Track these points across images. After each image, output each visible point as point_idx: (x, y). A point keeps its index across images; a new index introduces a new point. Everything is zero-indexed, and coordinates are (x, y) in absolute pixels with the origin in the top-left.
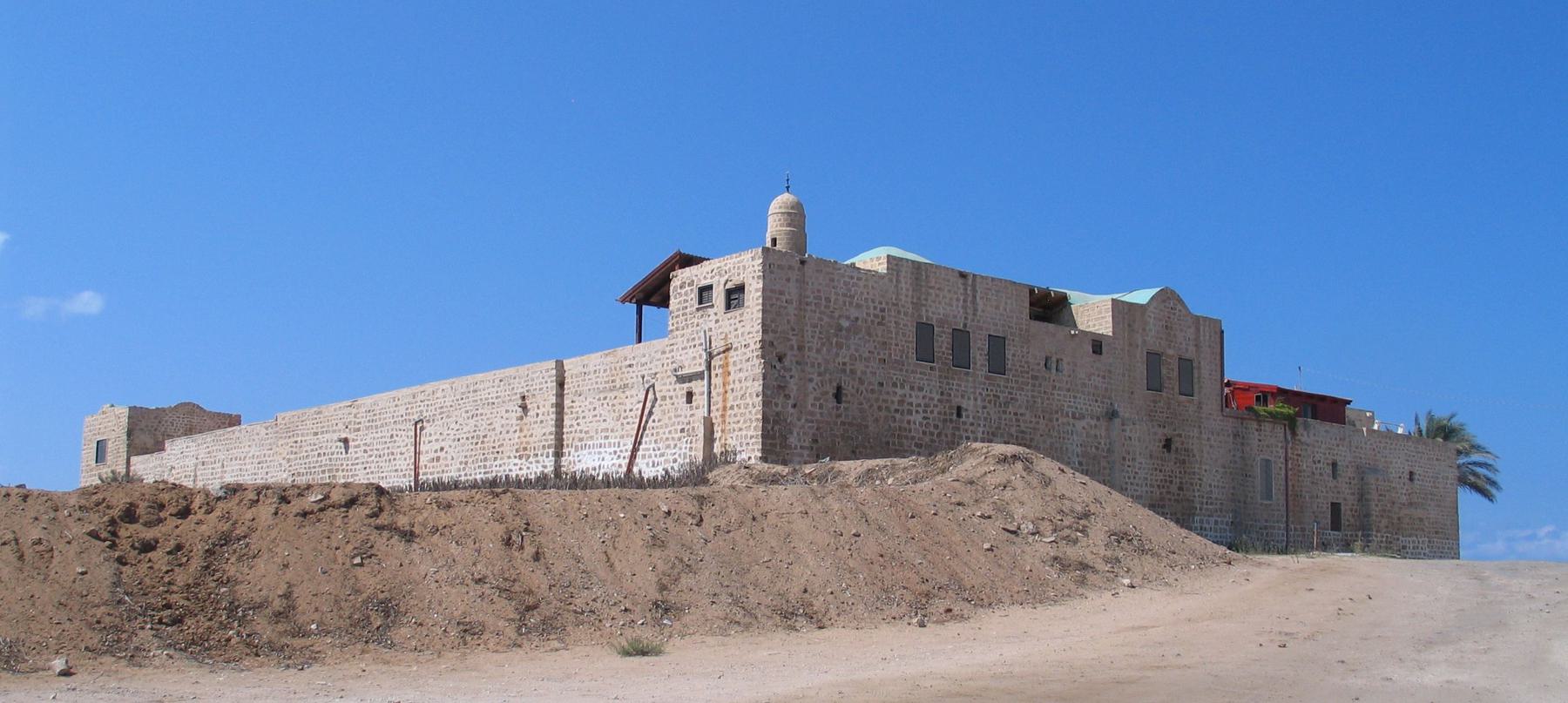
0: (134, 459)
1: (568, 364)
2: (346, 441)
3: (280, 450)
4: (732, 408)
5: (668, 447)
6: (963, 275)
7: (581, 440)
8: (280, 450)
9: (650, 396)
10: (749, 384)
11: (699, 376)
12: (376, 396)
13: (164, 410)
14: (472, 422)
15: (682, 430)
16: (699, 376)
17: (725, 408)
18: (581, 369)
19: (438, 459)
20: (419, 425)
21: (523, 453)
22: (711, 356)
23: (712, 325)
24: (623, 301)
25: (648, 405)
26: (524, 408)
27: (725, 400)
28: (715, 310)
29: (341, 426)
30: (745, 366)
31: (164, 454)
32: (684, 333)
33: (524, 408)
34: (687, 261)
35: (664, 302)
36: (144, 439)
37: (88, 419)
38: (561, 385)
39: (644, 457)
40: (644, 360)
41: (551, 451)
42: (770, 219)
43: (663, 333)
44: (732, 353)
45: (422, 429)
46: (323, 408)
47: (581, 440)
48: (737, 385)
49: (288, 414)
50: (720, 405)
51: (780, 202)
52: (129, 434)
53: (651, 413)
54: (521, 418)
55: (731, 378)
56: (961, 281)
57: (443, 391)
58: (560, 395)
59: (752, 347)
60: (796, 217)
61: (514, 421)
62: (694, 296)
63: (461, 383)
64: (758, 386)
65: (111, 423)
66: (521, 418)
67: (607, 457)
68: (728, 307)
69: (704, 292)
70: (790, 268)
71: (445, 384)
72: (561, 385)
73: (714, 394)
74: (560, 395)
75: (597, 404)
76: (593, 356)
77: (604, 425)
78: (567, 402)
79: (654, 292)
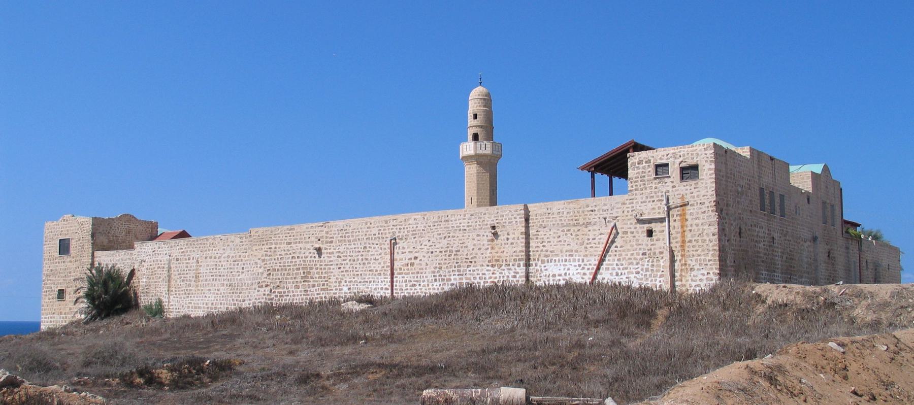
0: (97, 253)
1: (531, 207)
2: (319, 250)
3: (255, 253)
4: (690, 241)
5: (631, 263)
6: (772, 159)
7: (546, 256)
8: (255, 253)
9: (614, 231)
10: (706, 227)
11: (661, 220)
12: (348, 221)
13: (113, 219)
14: (445, 241)
15: (644, 254)
16: (661, 220)
17: (683, 242)
18: (545, 211)
19: (412, 264)
20: (393, 243)
21: (494, 263)
22: (669, 209)
23: (670, 189)
24: (583, 168)
25: (612, 237)
26: (496, 235)
27: (683, 236)
28: (671, 179)
29: (313, 239)
30: (701, 216)
31: (134, 252)
32: (642, 192)
33: (496, 235)
34: (638, 147)
35: (624, 174)
36: (103, 239)
37: (48, 224)
38: (527, 220)
39: (607, 269)
40: (605, 208)
41: (522, 263)
42: (470, 103)
43: (625, 191)
44: (688, 207)
45: (396, 243)
46: (296, 227)
47: (546, 256)
48: (694, 227)
49: (261, 230)
50: (679, 239)
51: (477, 92)
52: (93, 235)
53: (613, 242)
54: (492, 240)
55: (688, 223)
56: (770, 161)
57: (415, 220)
58: (527, 227)
59: (707, 204)
60: (487, 101)
61: (486, 242)
62: (652, 169)
63: (432, 216)
64: (714, 229)
65: (78, 228)
66: (492, 240)
67: (572, 268)
68: (682, 178)
69: (661, 169)
70: (722, 156)
71: (418, 216)
72: (527, 220)
73: (673, 232)
74: (527, 227)
75: (560, 233)
76: (556, 203)
77: (568, 248)
78: (532, 231)
79: (614, 166)
